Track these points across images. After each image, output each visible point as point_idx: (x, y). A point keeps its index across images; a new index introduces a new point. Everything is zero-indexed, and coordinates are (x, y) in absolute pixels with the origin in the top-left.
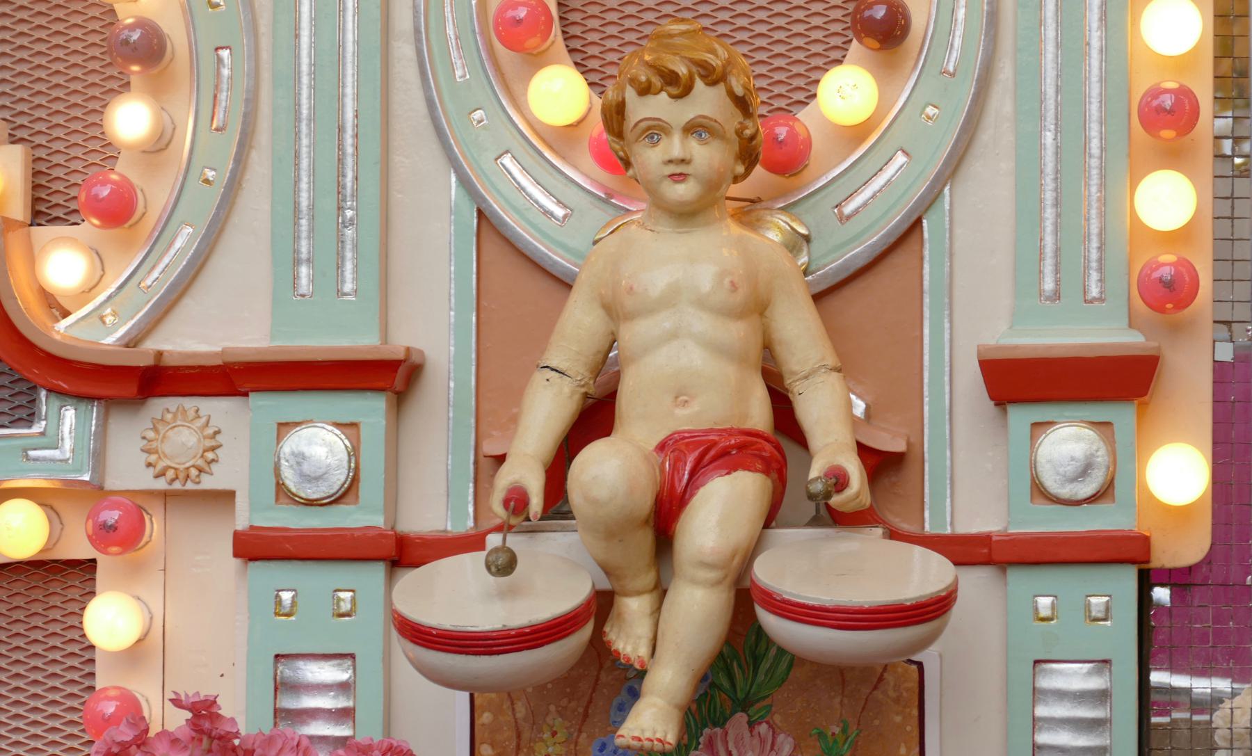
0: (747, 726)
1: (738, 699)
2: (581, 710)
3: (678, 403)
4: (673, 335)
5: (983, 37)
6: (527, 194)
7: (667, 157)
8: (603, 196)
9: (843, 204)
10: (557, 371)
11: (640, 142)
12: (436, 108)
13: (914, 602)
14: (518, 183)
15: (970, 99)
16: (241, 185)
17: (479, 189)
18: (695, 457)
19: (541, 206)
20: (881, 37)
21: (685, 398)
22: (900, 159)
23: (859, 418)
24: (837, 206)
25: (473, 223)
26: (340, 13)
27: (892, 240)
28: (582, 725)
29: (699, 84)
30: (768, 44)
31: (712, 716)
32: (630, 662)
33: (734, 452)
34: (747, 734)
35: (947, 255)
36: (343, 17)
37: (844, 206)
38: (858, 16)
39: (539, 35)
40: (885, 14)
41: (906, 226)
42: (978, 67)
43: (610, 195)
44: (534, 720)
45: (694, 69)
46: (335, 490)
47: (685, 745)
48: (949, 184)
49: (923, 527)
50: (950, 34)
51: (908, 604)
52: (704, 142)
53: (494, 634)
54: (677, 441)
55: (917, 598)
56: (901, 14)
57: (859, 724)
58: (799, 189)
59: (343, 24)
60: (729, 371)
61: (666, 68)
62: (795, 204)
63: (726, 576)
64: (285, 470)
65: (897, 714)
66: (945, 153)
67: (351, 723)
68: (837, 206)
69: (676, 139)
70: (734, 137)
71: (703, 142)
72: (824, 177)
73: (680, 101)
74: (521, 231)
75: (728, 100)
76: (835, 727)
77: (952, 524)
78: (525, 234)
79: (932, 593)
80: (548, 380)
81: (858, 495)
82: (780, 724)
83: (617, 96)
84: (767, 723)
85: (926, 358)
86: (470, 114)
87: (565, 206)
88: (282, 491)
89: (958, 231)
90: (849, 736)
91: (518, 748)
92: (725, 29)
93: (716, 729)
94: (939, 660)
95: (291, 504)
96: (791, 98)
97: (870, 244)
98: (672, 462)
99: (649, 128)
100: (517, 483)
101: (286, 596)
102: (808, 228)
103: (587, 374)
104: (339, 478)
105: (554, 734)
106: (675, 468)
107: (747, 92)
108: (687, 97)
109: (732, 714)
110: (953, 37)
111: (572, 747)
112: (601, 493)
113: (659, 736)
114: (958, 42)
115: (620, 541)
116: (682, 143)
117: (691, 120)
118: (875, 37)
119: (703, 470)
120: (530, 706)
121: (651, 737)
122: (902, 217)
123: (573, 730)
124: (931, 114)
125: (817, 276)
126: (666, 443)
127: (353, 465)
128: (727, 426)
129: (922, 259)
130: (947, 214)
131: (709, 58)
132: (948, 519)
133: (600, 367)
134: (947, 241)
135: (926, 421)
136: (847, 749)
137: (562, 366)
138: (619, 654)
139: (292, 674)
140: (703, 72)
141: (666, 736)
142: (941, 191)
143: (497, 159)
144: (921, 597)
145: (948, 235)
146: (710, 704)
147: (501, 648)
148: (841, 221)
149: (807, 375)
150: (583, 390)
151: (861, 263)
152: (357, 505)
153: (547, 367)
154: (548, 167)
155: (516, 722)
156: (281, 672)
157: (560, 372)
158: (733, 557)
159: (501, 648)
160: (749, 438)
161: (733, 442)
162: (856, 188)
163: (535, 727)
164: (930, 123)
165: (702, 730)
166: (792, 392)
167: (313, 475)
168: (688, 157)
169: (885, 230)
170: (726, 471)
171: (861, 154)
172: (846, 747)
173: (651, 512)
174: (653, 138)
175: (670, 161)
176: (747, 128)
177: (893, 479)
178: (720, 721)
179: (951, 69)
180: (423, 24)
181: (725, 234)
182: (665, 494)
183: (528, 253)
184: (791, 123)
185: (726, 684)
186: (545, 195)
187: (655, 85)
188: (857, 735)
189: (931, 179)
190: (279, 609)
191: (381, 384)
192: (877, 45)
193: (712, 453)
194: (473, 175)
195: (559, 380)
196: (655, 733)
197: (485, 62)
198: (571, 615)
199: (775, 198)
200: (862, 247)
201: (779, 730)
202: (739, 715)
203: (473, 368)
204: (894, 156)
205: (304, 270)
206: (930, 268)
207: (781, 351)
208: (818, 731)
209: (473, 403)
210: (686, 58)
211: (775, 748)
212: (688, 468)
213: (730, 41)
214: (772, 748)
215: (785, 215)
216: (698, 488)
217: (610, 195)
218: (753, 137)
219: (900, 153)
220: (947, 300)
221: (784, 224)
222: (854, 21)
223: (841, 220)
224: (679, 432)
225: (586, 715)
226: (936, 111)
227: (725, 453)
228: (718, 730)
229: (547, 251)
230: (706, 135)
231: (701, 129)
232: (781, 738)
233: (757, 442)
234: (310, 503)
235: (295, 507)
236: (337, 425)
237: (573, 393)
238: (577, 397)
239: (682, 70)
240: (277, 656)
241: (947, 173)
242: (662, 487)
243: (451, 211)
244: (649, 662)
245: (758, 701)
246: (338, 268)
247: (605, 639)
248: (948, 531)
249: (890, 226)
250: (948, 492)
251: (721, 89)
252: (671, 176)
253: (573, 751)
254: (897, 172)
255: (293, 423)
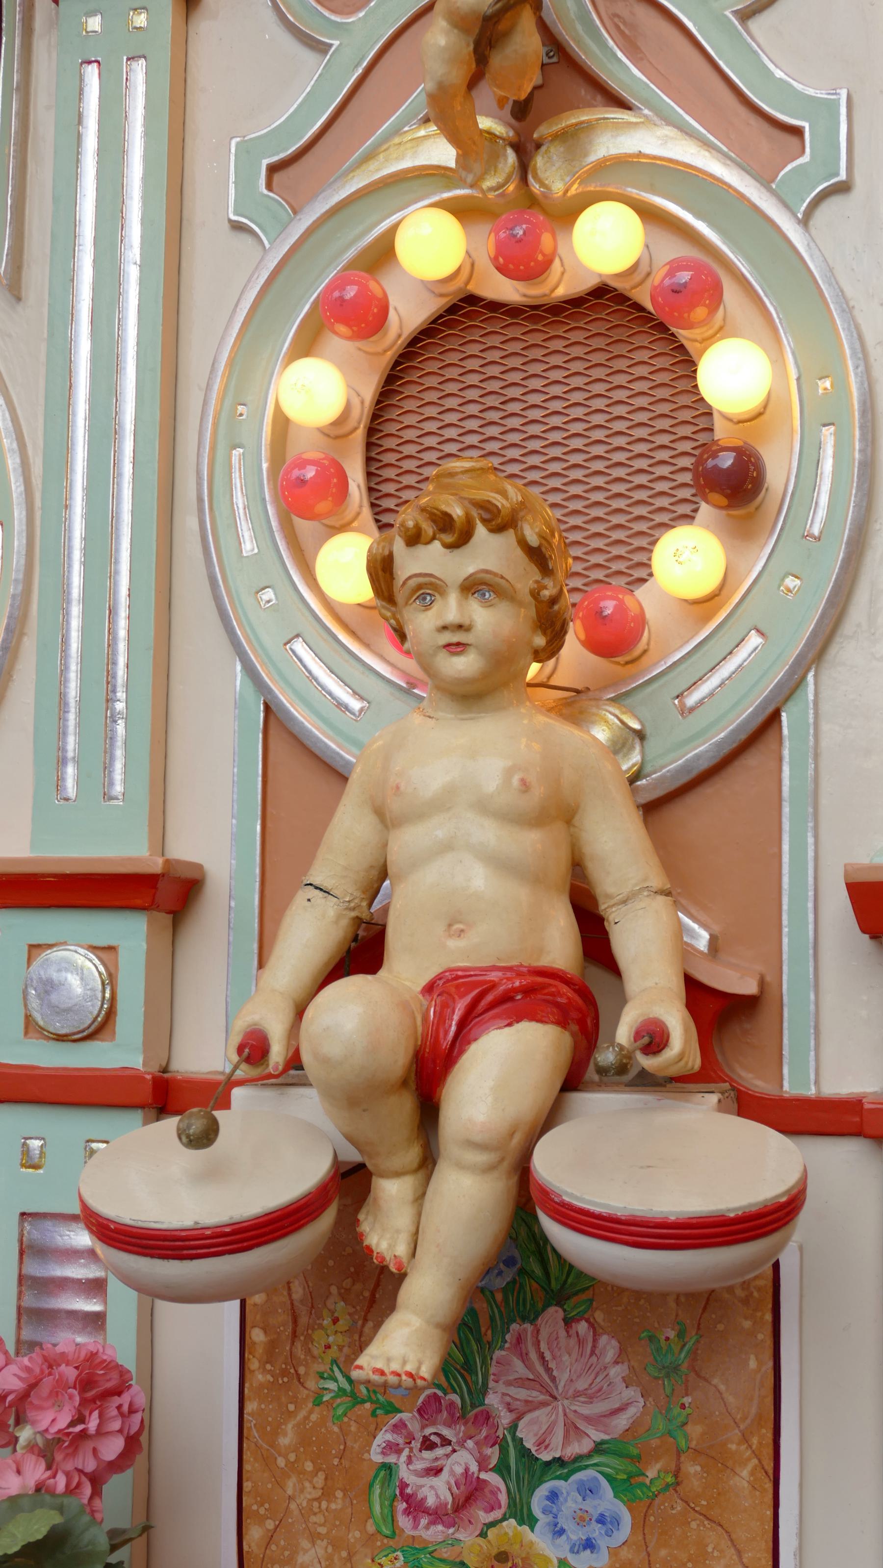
0: (563, 1324)
1: (552, 1291)
2: (367, 1294)
3: (452, 932)
4: (446, 847)
5: (854, 492)
6: (319, 684)
7: (440, 623)
8: (404, 685)
9: (686, 693)
10: (321, 890)
11: (411, 604)
12: (219, 586)
13: (740, 1213)
14: (310, 672)
15: (838, 566)
16: (11, 676)
17: (263, 677)
18: (465, 1004)
19: (334, 698)
20: (729, 491)
21: (461, 926)
22: (754, 640)
23: (702, 951)
24: (678, 697)
25: (260, 717)
26: (114, 480)
27: (743, 737)
28: (368, 1311)
29: (481, 531)
30: (606, 514)
31: (521, 1309)
32: (385, 1263)
33: (519, 997)
34: (562, 1333)
35: (811, 755)
36: (118, 485)
37: (687, 696)
38: (701, 468)
39: (330, 499)
40: (732, 464)
41: (761, 719)
42: (848, 527)
43: (412, 684)
44: (312, 1304)
45: (474, 513)
46: (86, 1025)
47: (489, 1343)
48: (813, 670)
49: (782, 1086)
50: (815, 489)
51: (732, 1215)
52: (489, 604)
53: (184, 1234)
54: (448, 981)
55: (745, 1207)
56: (753, 465)
57: (699, 1328)
58: (634, 678)
59: (117, 493)
60: (522, 893)
61: (437, 510)
62: (627, 694)
63: (502, 1160)
64: (32, 1000)
65: (746, 1318)
66: (807, 631)
67: (104, 1295)
68: (678, 697)
69: (453, 598)
70: (529, 599)
71: (488, 605)
72: (663, 663)
73: (457, 552)
74: (310, 726)
75: (519, 552)
76: (669, 1330)
77: (817, 1082)
78: (314, 730)
79: (766, 1200)
80: (309, 900)
81: (681, 1056)
82: (602, 1323)
83: (383, 550)
84: (587, 1321)
85: (785, 880)
86: (257, 593)
87: (362, 698)
88: (30, 1024)
89: (825, 727)
90: (687, 1343)
91: (294, 1335)
92: (514, 469)
93: (525, 1325)
94: (798, 1253)
95: (42, 1038)
96: (632, 576)
97: (717, 741)
98: (438, 1009)
99: (420, 587)
100: (255, 1025)
101: (35, 1144)
102: (641, 722)
103: (358, 894)
104: (94, 1009)
105: (335, 1321)
106: (442, 1018)
107: (544, 542)
108: (464, 547)
109: (544, 1309)
110: (818, 493)
111: (356, 1337)
112: (333, 1049)
113: (408, 1368)
114: (824, 499)
115: (364, 1110)
116: (460, 606)
117: (471, 575)
118: (722, 492)
119: (477, 1020)
120: (308, 1286)
121: (399, 1371)
122: (755, 710)
123: (357, 1317)
124: (791, 586)
125: (653, 779)
126: (435, 982)
127: (107, 995)
128: (514, 963)
129: (780, 759)
130: (811, 705)
131: (499, 501)
132: (812, 1077)
133: (376, 886)
134: (811, 738)
135: (785, 956)
136: (685, 1358)
137: (327, 884)
138: (372, 1251)
139: (39, 1237)
140: (486, 516)
141: (419, 1368)
142: (804, 677)
143: (286, 644)
144: (750, 1205)
145: (812, 731)
146: (519, 1293)
147: (194, 1252)
148: (682, 714)
149: (625, 899)
150: (353, 914)
151: (704, 765)
152: (114, 1042)
153: (311, 884)
154: (343, 652)
155: (292, 1304)
156: (29, 1233)
157: (325, 892)
158: (512, 1135)
159: (194, 1252)
160: (539, 979)
161: (517, 984)
162: (701, 674)
163: (313, 1312)
164: (790, 597)
165: (508, 1324)
166: (608, 921)
167: (62, 1006)
168: (466, 622)
169: (735, 724)
170: (507, 1022)
171: (707, 634)
172: (682, 1355)
173: (409, 1070)
174: (425, 599)
175: (445, 628)
176: (545, 588)
177: (747, 1026)
178: (531, 1316)
179: (816, 531)
180: (206, 491)
181: (525, 722)
182: (427, 1050)
183: (317, 752)
184: (621, 596)
185: (538, 1271)
186: (340, 686)
187: (426, 532)
188: (698, 1341)
189: (790, 663)
190: (30, 1162)
191: (139, 902)
192: (724, 501)
193: (490, 998)
194: (258, 662)
195: (323, 901)
196: (404, 1362)
197: (275, 533)
198: (302, 1202)
199: (605, 688)
200: (707, 745)
201: (601, 1331)
202: (552, 1310)
203: (257, 885)
204: (746, 636)
205: (70, 770)
206: (790, 770)
207: (595, 871)
208: (650, 1334)
209: (256, 925)
210: (465, 499)
211: (597, 1352)
212: (456, 1018)
213: (521, 482)
214: (593, 1353)
215: (613, 706)
216: (469, 1043)
217: (412, 684)
218: (554, 601)
219: (753, 632)
220: (811, 810)
221: (612, 717)
222: (696, 478)
223: (683, 713)
224: (451, 970)
225: (372, 1301)
226: (798, 582)
227: (507, 998)
228: (528, 1326)
229: (338, 750)
230: (490, 595)
231: (484, 587)
232: (604, 1340)
233: (550, 985)
234: (61, 1038)
235: (45, 1042)
236: (93, 949)
237: (339, 917)
238: (345, 922)
239: (457, 512)
240: (23, 1214)
241: (810, 656)
242: (424, 1037)
243: (236, 703)
244: (409, 1262)
245: (576, 1293)
246: (105, 768)
247: (357, 1229)
248: (811, 1092)
249: (740, 719)
250: (812, 1043)
251: (510, 536)
252: (448, 646)
253: (357, 1343)
254: (750, 655)
255: (45, 945)
